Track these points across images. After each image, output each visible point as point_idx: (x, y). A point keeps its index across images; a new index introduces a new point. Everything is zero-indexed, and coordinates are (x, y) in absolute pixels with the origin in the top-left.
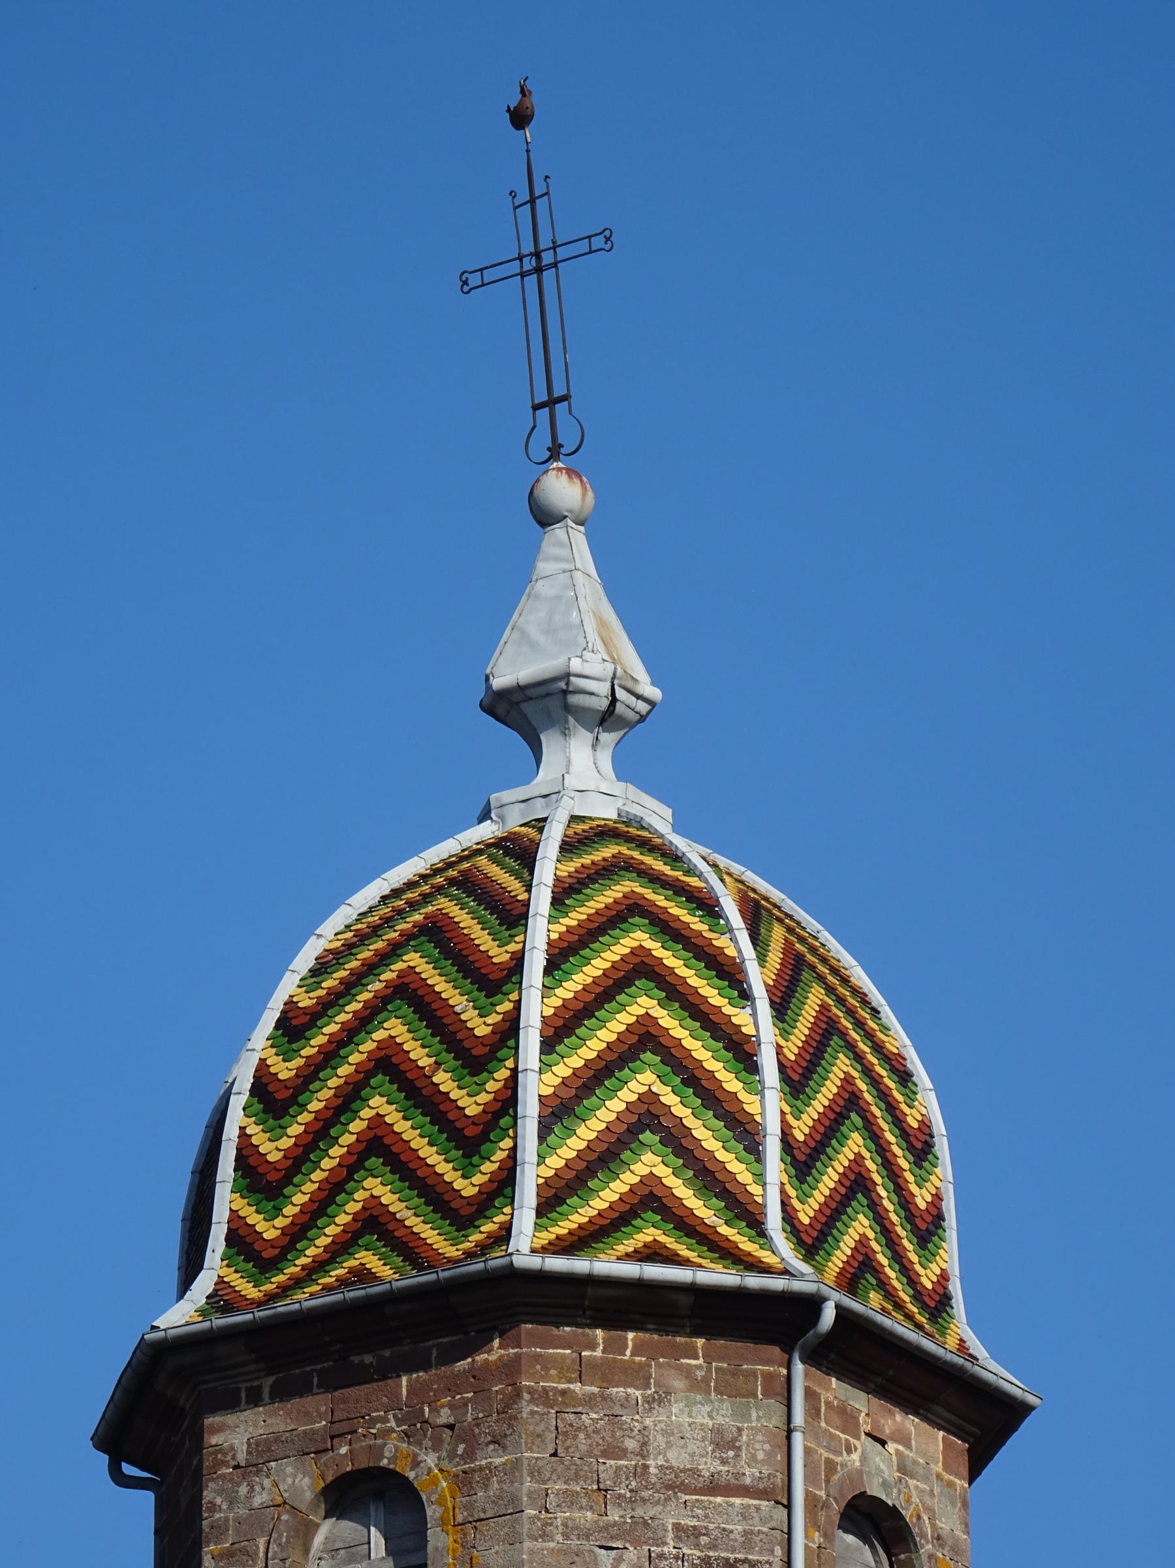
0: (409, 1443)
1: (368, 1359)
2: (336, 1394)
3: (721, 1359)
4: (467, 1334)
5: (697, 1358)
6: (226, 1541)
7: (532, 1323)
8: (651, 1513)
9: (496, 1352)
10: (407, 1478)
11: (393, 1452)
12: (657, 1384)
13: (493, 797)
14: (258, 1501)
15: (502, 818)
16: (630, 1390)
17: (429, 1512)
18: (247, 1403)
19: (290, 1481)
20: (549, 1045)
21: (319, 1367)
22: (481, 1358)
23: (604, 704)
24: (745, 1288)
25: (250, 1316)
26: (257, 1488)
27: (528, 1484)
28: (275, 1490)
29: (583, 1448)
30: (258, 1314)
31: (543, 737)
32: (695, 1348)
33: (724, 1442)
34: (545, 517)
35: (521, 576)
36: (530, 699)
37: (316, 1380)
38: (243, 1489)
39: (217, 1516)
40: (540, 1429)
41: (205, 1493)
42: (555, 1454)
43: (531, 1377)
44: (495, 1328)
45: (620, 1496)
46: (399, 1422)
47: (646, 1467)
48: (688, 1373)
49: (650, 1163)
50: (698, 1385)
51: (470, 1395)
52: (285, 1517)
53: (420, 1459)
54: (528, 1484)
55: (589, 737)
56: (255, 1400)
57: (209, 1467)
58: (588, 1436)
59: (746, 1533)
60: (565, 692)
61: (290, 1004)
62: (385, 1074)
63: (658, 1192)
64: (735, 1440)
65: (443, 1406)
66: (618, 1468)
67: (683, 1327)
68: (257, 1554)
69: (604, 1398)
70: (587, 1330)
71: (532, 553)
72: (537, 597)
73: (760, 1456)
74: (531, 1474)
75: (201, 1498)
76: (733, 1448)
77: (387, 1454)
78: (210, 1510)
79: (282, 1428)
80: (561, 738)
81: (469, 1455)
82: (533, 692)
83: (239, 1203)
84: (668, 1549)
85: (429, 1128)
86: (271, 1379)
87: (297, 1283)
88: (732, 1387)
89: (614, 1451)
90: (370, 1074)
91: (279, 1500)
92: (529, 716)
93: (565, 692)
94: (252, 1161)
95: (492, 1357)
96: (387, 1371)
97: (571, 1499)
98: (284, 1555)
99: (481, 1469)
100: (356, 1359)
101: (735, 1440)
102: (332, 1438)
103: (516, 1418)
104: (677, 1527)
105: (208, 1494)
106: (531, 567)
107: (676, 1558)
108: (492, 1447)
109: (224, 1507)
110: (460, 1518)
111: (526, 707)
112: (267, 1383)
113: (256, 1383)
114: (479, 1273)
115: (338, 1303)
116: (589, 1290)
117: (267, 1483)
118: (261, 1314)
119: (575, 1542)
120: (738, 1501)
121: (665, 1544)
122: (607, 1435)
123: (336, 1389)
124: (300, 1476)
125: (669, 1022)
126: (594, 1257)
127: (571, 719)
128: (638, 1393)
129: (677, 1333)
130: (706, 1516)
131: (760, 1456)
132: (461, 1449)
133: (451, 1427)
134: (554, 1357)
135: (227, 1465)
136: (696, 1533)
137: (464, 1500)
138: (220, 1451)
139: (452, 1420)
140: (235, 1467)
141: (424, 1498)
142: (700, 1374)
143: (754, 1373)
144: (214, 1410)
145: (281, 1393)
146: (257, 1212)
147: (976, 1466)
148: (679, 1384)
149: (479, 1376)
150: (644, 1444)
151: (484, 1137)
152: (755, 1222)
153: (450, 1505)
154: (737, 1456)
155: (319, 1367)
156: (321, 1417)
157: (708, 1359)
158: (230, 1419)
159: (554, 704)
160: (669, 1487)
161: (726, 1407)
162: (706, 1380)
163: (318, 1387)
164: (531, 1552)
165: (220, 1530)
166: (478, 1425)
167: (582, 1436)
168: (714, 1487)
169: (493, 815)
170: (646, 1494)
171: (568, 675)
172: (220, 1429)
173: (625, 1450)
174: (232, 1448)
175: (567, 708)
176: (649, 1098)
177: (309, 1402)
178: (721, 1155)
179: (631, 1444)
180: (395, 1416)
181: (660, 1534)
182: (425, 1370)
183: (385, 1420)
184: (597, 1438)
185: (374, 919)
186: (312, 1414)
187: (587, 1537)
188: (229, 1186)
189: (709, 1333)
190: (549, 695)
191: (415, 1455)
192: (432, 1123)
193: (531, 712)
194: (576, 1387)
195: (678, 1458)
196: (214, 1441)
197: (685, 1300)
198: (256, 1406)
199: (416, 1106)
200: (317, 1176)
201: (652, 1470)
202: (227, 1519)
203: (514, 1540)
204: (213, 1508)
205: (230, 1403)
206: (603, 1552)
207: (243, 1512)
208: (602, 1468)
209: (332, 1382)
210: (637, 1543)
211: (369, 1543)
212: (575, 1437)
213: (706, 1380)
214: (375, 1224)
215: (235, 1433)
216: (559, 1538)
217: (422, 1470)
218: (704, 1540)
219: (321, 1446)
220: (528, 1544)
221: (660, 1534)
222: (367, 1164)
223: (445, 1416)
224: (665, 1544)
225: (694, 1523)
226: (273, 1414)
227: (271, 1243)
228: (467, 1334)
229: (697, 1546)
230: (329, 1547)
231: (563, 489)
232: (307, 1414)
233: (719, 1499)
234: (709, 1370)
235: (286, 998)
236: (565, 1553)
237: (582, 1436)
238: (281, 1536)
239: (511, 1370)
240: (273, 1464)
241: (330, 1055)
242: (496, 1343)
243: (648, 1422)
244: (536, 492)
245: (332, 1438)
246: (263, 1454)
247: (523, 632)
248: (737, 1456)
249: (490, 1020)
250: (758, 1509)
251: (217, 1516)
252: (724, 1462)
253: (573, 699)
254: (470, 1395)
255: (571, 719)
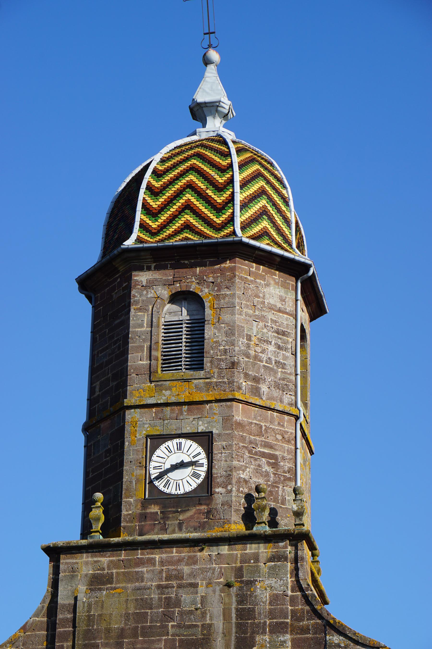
0: (199, 285)
1: (186, 262)
2: (176, 270)
3: (282, 278)
4: (218, 258)
5: (276, 276)
6: (139, 305)
7: (239, 258)
8: (265, 314)
9: (228, 264)
10: (199, 295)
11: (194, 287)
12: (267, 281)
13: (197, 130)
14: (149, 296)
15: (200, 136)
16: (261, 281)
17: (206, 304)
18: (146, 269)
19: (160, 292)
20: (242, 187)
21: (170, 262)
22: (223, 265)
23: (227, 112)
24: (295, 259)
25: (156, 245)
26: (149, 292)
27: (237, 300)
28: (155, 293)
29: (250, 293)
30: (159, 244)
31: (207, 118)
32: (276, 274)
33: (283, 300)
34: (207, 62)
35: (201, 77)
36: (207, 106)
37: (169, 266)
38: (145, 292)
39: (136, 298)
40: (240, 286)
41: (132, 292)
42: (243, 294)
43: (238, 272)
44: (228, 258)
45: (258, 308)
46: (196, 279)
47: (264, 302)
48: (274, 280)
49: (265, 224)
50: (277, 283)
51: (219, 275)
52: (158, 301)
53: (203, 290)
54: (237, 300)
55: (220, 120)
56: (149, 269)
57: (133, 285)
58: (251, 291)
59: (287, 324)
60: (218, 106)
61: (155, 168)
62: (190, 189)
63: (267, 231)
64: (285, 300)
65: (210, 277)
66: (258, 301)
67: (274, 267)
68: (149, 310)
69: (255, 282)
70: (251, 263)
71: (204, 71)
72: (207, 82)
73: (291, 305)
74: (238, 297)
75: (131, 293)
76: (284, 302)
77: (192, 287)
78: (133, 297)
79: (158, 277)
80: (213, 119)
81: (219, 290)
82: (208, 105)
83: (143, 217)
84: (269, 324)
85: (205, 204)
86: (155, 264)
87: (170, 237)
88: (284, 286)
89: (257, 296)
90: (184, 189)
91: (156, 296)
92: (205, 112)
93: (218, 106)
94: (148, 206)
95: (227, 266)
96: (193, 266)
97: (247, 306)
98: (158, 311)
99: (222, 294)
100: (182, 262)
101: (285, 300)
102: (174, 282)
103: (234, 282)
104: (271, 319)
105: (133, 292)
106: (204, 74)
107: (271, 327)
108: (226, 289)
109: (138, 296)
110: (215, 307)
111: (205, 109)
112: (153, 265)
113: (149, 265)
114: (231, 241)
115: (185, 244)
116: (256, 252)
117: (152, 291)
118: (160, 244)
119: (248, 318)
120: (285, 316)
121: (268, 323)
122: (256, 292)
123: (175, 269)
124: (163, 291)
125: (268, 188)
126: (261, 242)
127: (217, 114)
128: (263, 282)
129: (272, 269)
130: (278, 318)
131: (291, 305)
132: (216, 289)
133: (213, 283)
134: (244, 268)
135: (139, 285)
136: (276, 322)
137: (217, 302)
138: (137, 281)
139: (213, 281)
140: (142, 286)
141: (204, 300)
142: (277, 281)
143: (289, 283)
144: (135, 270)
145: (157, 268)
146: (149, 220)
147: (311, 321)
148: (272, 282)
149: (222, 271)
150: (264, 296)
151: (223, 208)
152: (290, 245)
153: (213, 303)
154: (285, 304)
155: (170, 262)
156: (170, 276)
157: (279, 278)
158: (141, 273)
159: (213, 109)
160: (270, 308)
161: (283, 290)
162: (278, 282)
163: (170, 268)
164: (238, 318)
165: (137, 302)
166: (222, 283)
167: (250, 290)
168: (280, 311)
169: (197, 134)
170: (264, 309)
171: (220, 101)
172: (137, 276)
173: (260, 296)
174: (141, 281)
175: (217, 111)
176: (264, 207)
177: (167, 271)
178: (282, 226)
179: (261, 295)
180: (195, 278)
181: (267, 320)
182: (205, 267)
183: (192, 279)
184: (253, 292)
185: (174, 152)
186: (168, 275)
187: (251, 317)
188: (140, 212)
189: (280, 271)
190: (213, 106)
191: (201, 289)
192: (206, 203)
193: (200, 112)
194: (249, 277)
195: (272, 301)
196: (135, 278)
197: (278, 259)
198: (149, 271)
199: (200, 198)
200: (169, 213)
201: (266, 303)
202: (139, 300)
203: (233, 314)
204: (135, 296)
205: (141, 269)
206: (254, 322)
207: (144, 298)
208: (254, 300)
209: (174, 267)
210: (262, 321)
211: (182, 311)
212: (248, 290)
213: (278, 282)
214: (187, 226)
215: (142, 277)
216: (244, 316)
217: (204, 293)
218: (277, 324)
219: (170, 284)
220: (237, 316)
221: (267, 320)
222: (185, 211)
223: (211, 279)
224: (268, 323)
225: (275, 319)
226: (156, 274)
227: (155, 229)
228: (218, 258)
229: (276, 325)
230: (169, 311)
231: (214, 55)
232: (166, 274)
233: (281, 314)
234: (279, 280)
235: (154, 167)
236: (246, 320)
237: (250, 290)
238: (157, 306)
239: (233, 270)
240: (155, 287)
241: (172, 182)
242: (228, 262)
243: (265, 290)
244: (207, 54)
245: (174, 282)
246: (150, 285)
247: (204, 89)
248: (285, 304)
249: (223, 178)
250: (290, 319)
251: (136, 298)
252: (282, 305)
253: (219, 109)
254: (219, 275)
255: (217, 114)
